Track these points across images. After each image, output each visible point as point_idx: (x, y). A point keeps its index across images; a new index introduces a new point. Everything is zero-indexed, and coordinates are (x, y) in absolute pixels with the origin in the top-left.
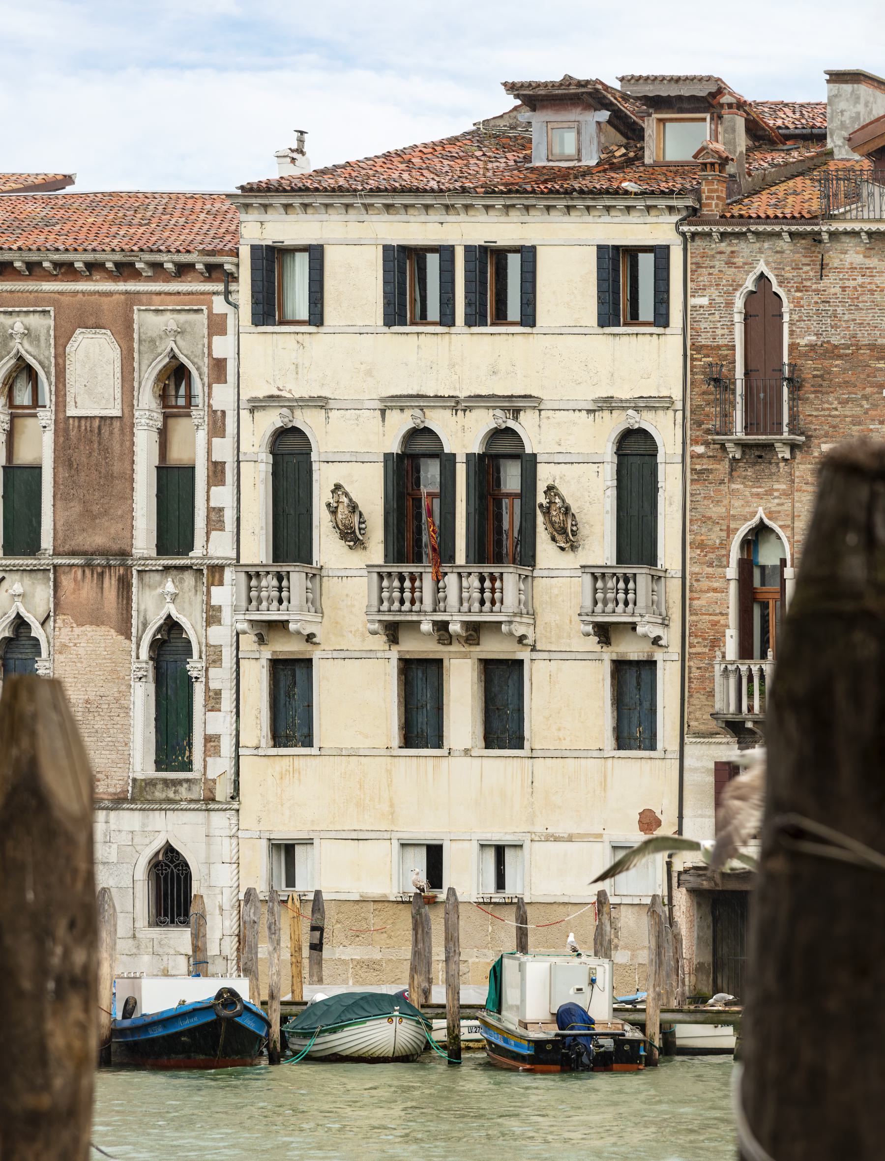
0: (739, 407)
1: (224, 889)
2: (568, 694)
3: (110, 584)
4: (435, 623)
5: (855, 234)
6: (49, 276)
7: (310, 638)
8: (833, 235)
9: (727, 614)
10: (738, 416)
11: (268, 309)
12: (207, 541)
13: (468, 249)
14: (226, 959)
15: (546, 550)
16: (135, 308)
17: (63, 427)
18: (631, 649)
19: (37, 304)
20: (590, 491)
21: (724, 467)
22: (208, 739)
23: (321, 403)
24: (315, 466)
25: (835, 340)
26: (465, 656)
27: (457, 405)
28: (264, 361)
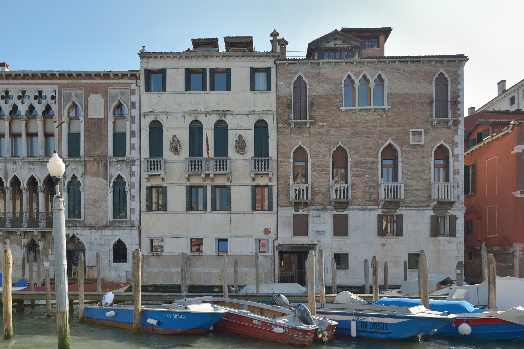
0: (293, 113)
13: (211, 69)
19: (79, 86)
21: (288, 130)
22: (131, 209)
23: (166, 114)
25: (323, 94)
27: (208, 114)
28: (150, 102)
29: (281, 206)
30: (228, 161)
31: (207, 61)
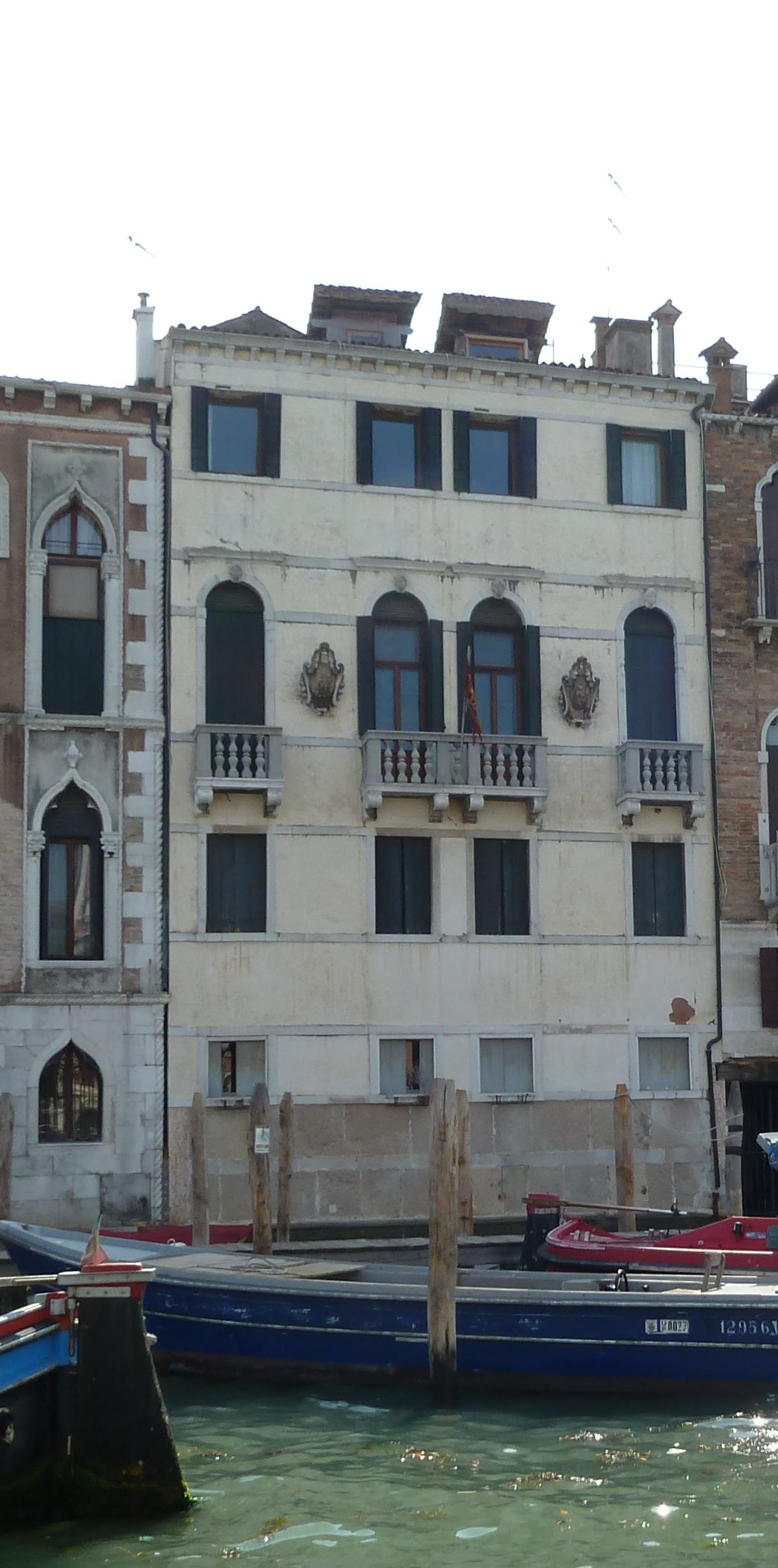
1: (148, 1096)
2: (581, 876)
4: (452, 797)
9: (759, 798)
10: (761, 603)
12: (124, 701)
14: (148, 1176)
16: (30, 441)
21: (749, 651)
23: (281, 560)
24: (268, 626)
26: (459, 834)
27: (450, 572)
28: (216, 514)
29: (733, 920)
30: (539, 750)
31: (441, 382)
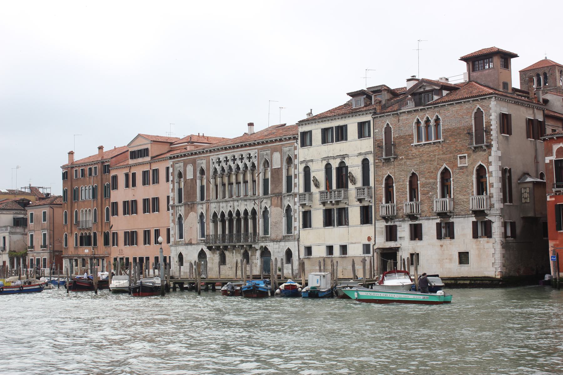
3: (279, 199)
5: (404, 112)
6: (270, 143)
7: (310, 206)
8: (400, 113)
10: (384, 153)
11: (303, 145)
15: (350, 185)
17: (272, 170)
18: (366, 204)
19: (267, 149)
20: (356, 171)
21: (381, 164)
25: (402, 135)
27: (334, 158)
